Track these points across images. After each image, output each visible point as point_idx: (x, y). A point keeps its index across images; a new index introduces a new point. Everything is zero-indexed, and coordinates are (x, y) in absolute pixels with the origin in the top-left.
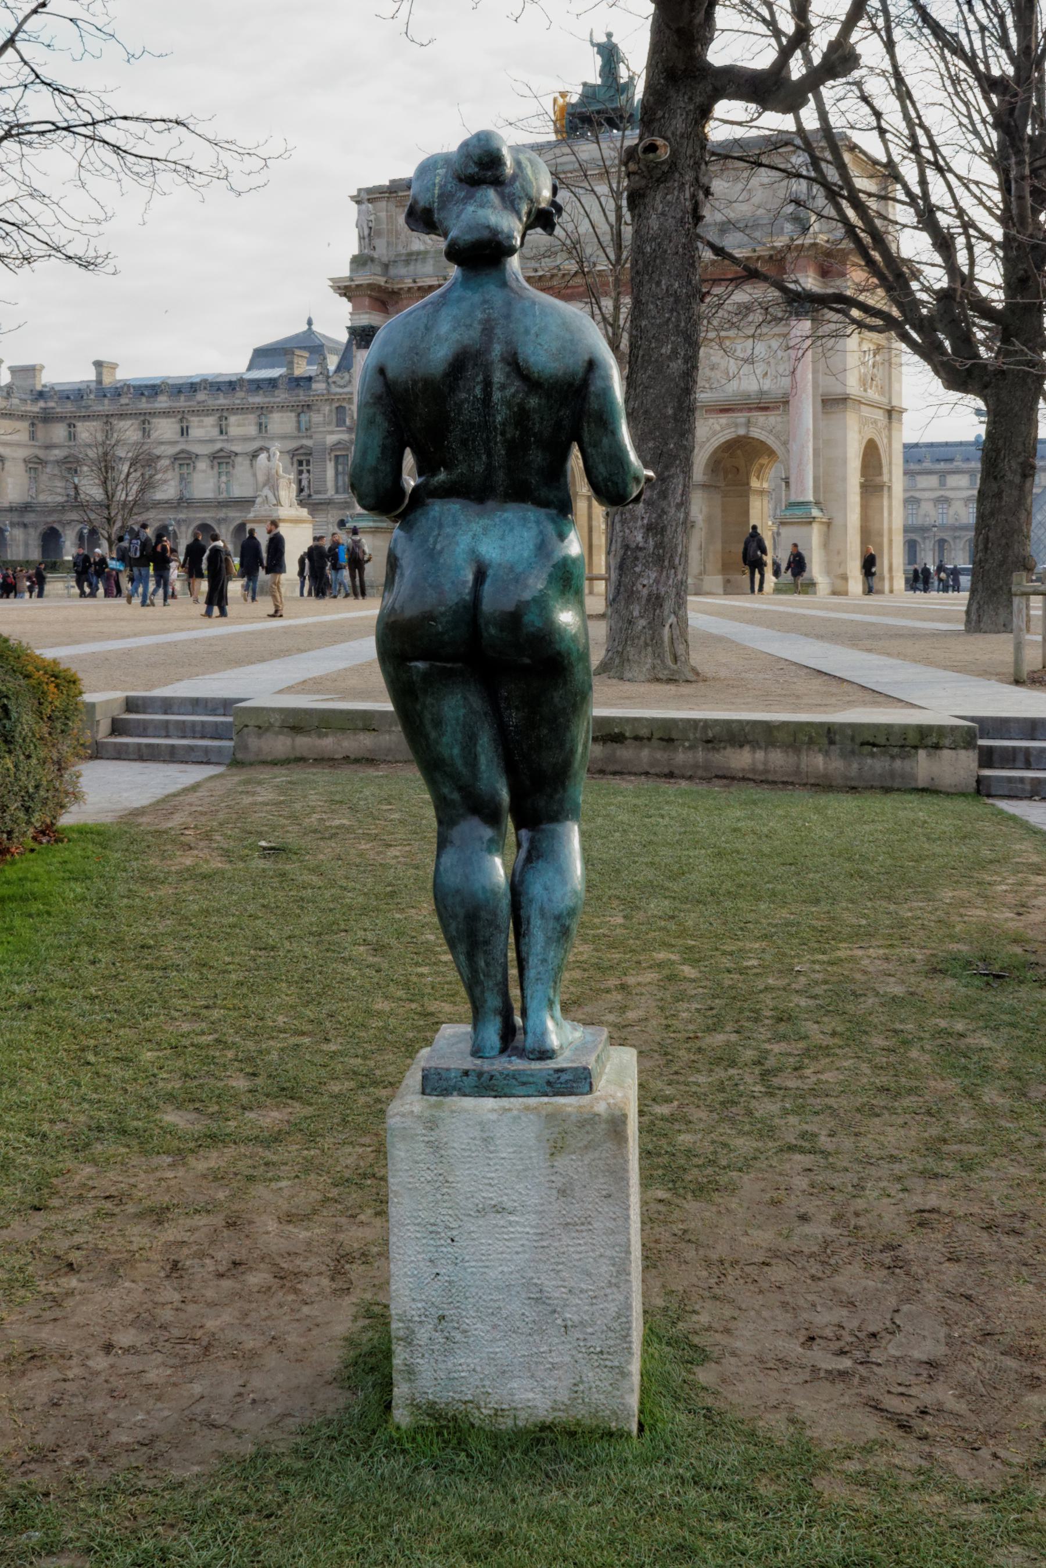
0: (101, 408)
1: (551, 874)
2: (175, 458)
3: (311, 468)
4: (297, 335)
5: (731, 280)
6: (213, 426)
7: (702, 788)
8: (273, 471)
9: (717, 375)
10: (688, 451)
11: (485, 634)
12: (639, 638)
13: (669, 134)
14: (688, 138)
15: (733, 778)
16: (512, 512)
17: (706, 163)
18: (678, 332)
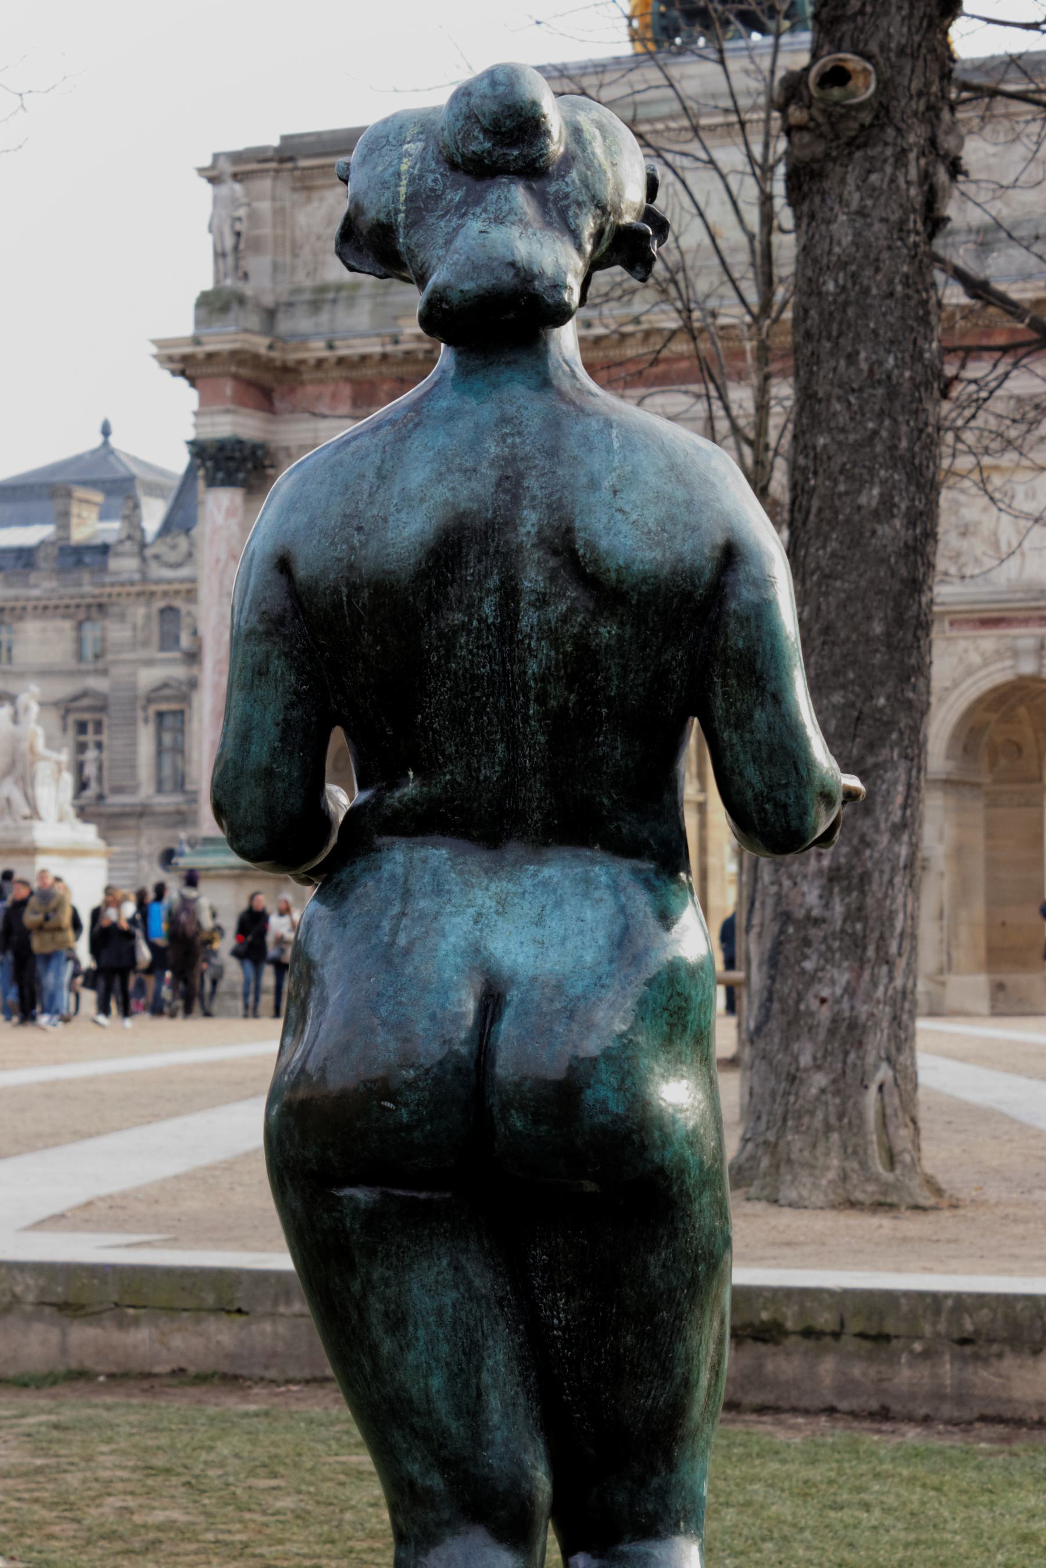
3: (104, 738)
4: (78, 459)
5: (1005, 350)
7: (952, 1442)
8: (24, 746)
9: (977, 546)
10: (919, 711)
11: (501, 1129)
12: (812, 1113)
13: (874, 48)
14: (914, 57)
15: (1019, 1422)
16: (558, 870)
17: (953, 109)
18: (895, 460)
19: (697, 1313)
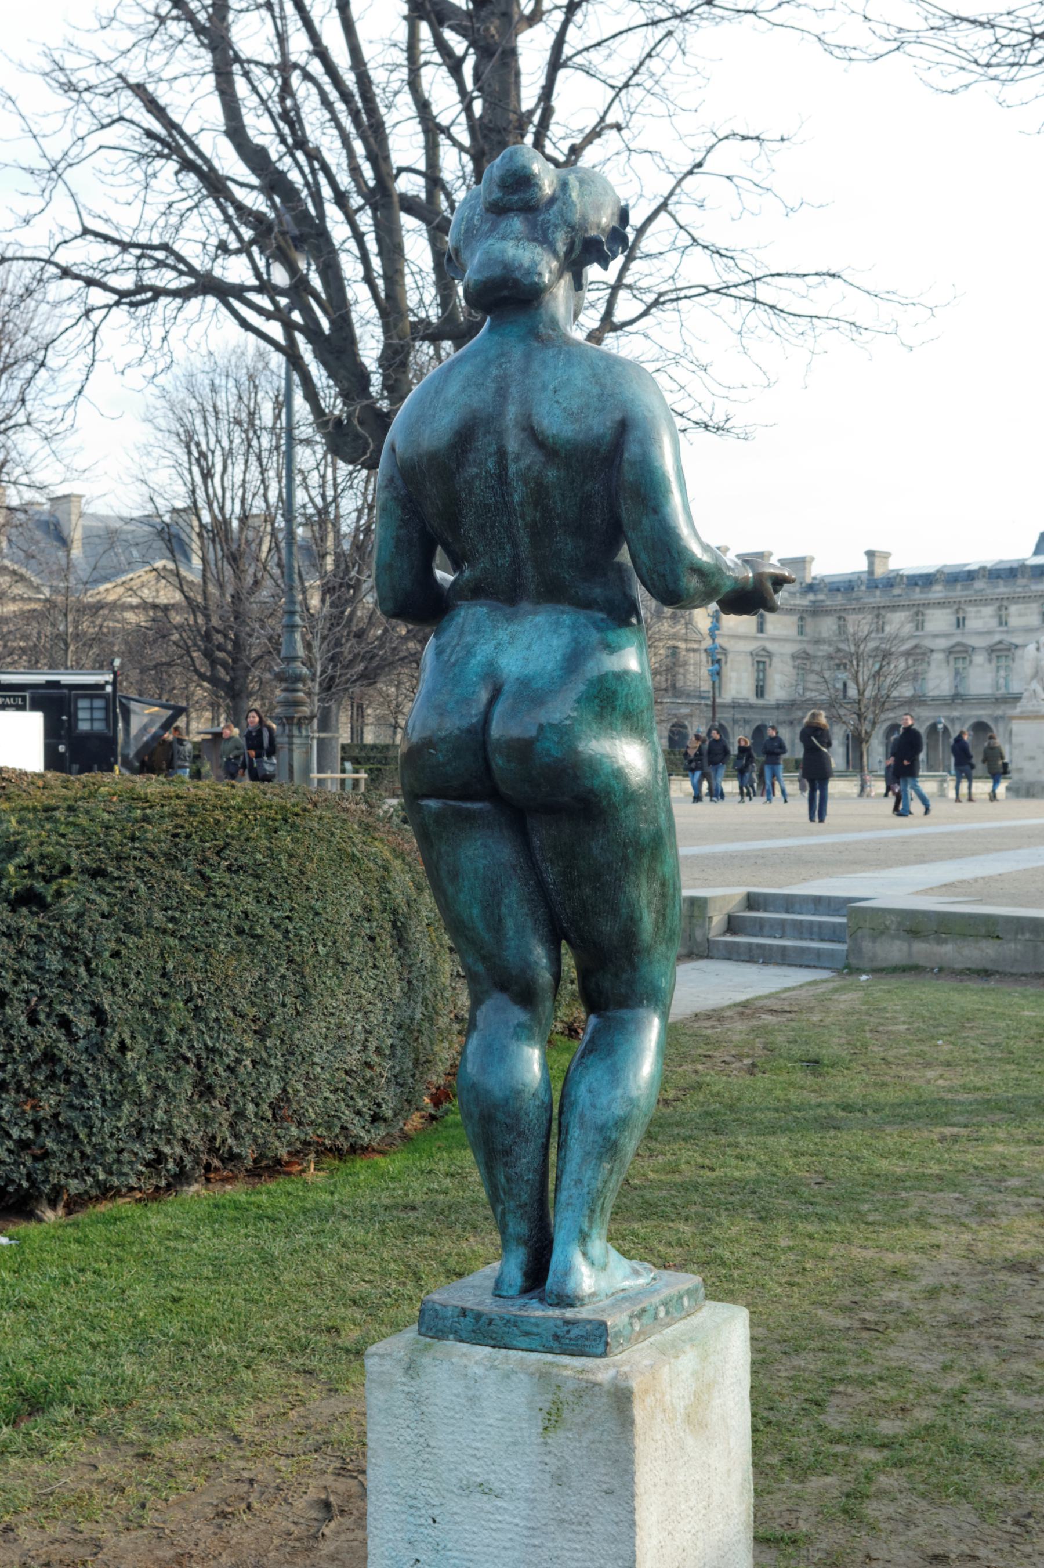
0: (872, 600)
1: (599, 1073)
2: (949, 651)
6: (992, 617)
19: (633, 877)
